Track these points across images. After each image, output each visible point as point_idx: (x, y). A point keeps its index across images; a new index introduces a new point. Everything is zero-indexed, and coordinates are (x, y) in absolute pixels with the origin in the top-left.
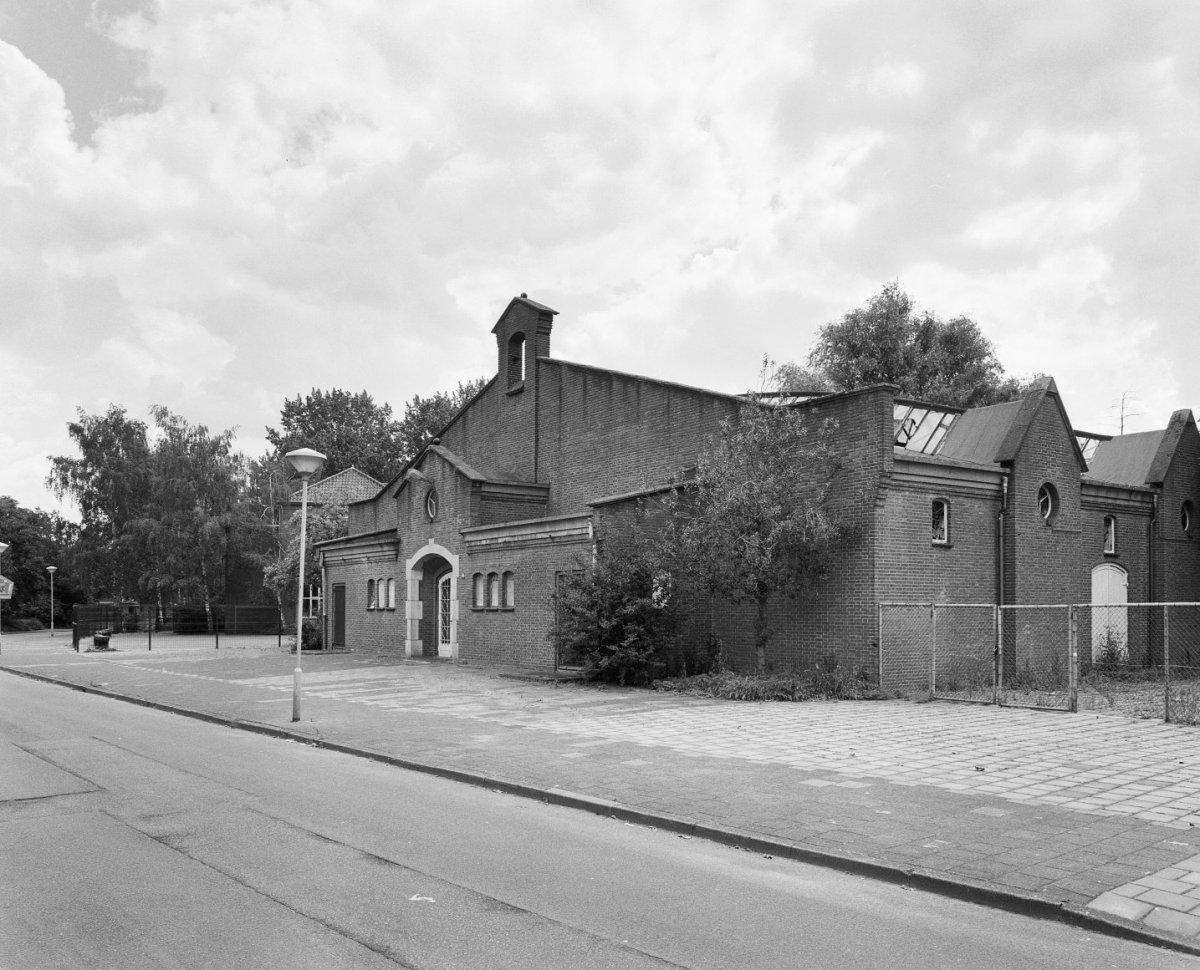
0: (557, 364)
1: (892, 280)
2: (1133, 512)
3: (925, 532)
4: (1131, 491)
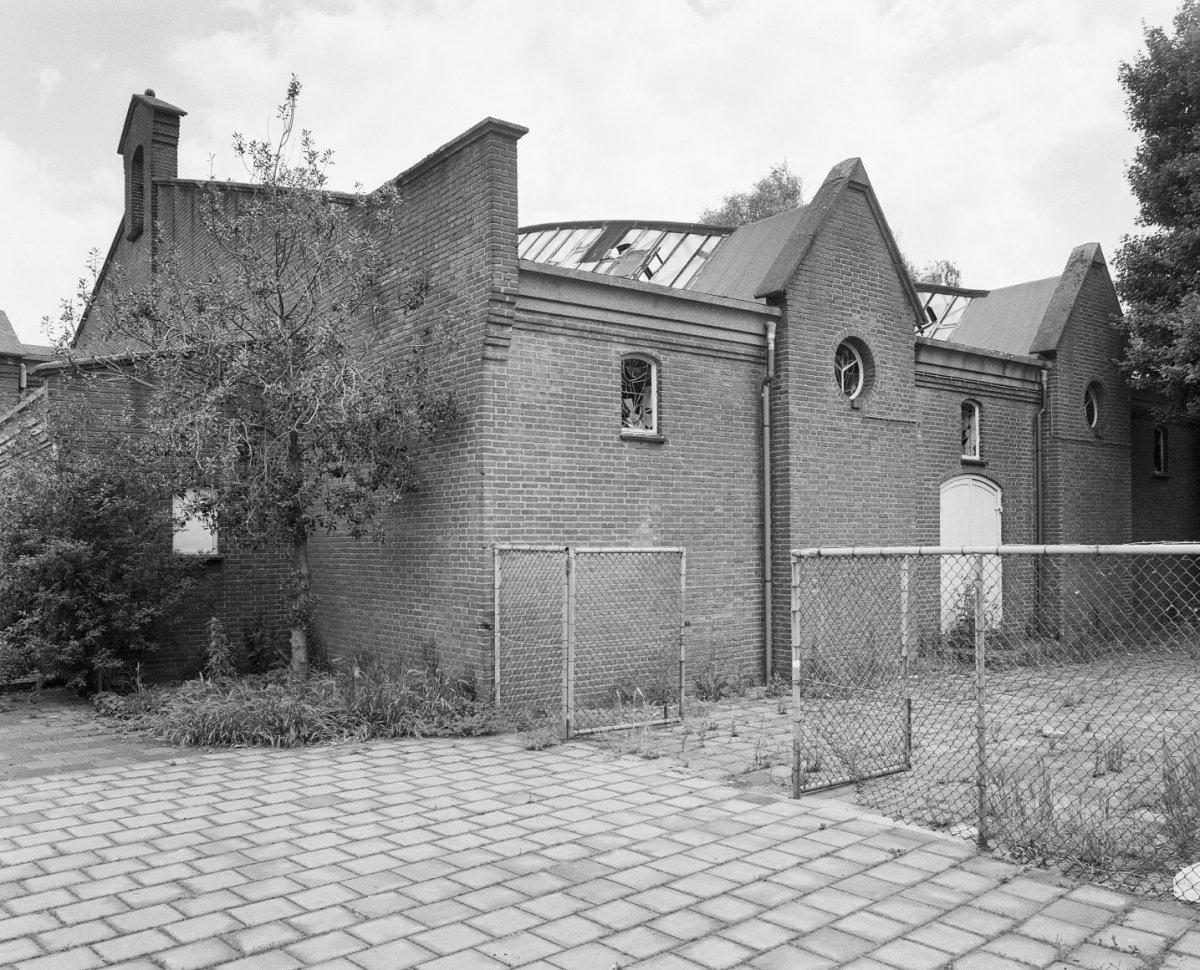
0: (189, 187)
1: (780, 162)
2: (1011, 395)
3: (603, 413)
4: (1005, 363)
